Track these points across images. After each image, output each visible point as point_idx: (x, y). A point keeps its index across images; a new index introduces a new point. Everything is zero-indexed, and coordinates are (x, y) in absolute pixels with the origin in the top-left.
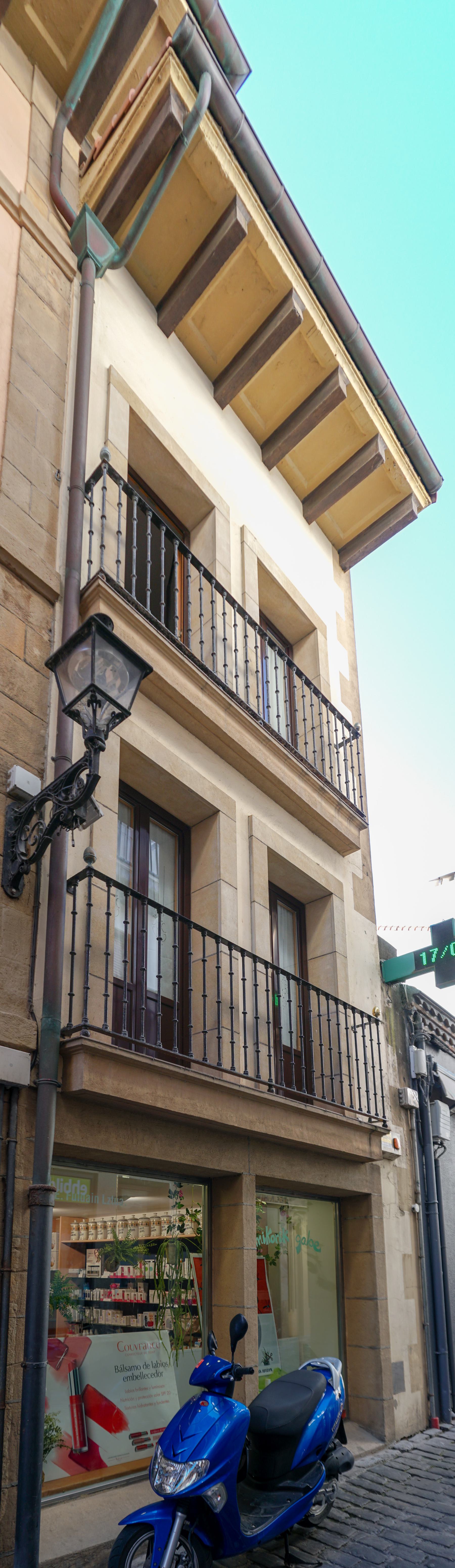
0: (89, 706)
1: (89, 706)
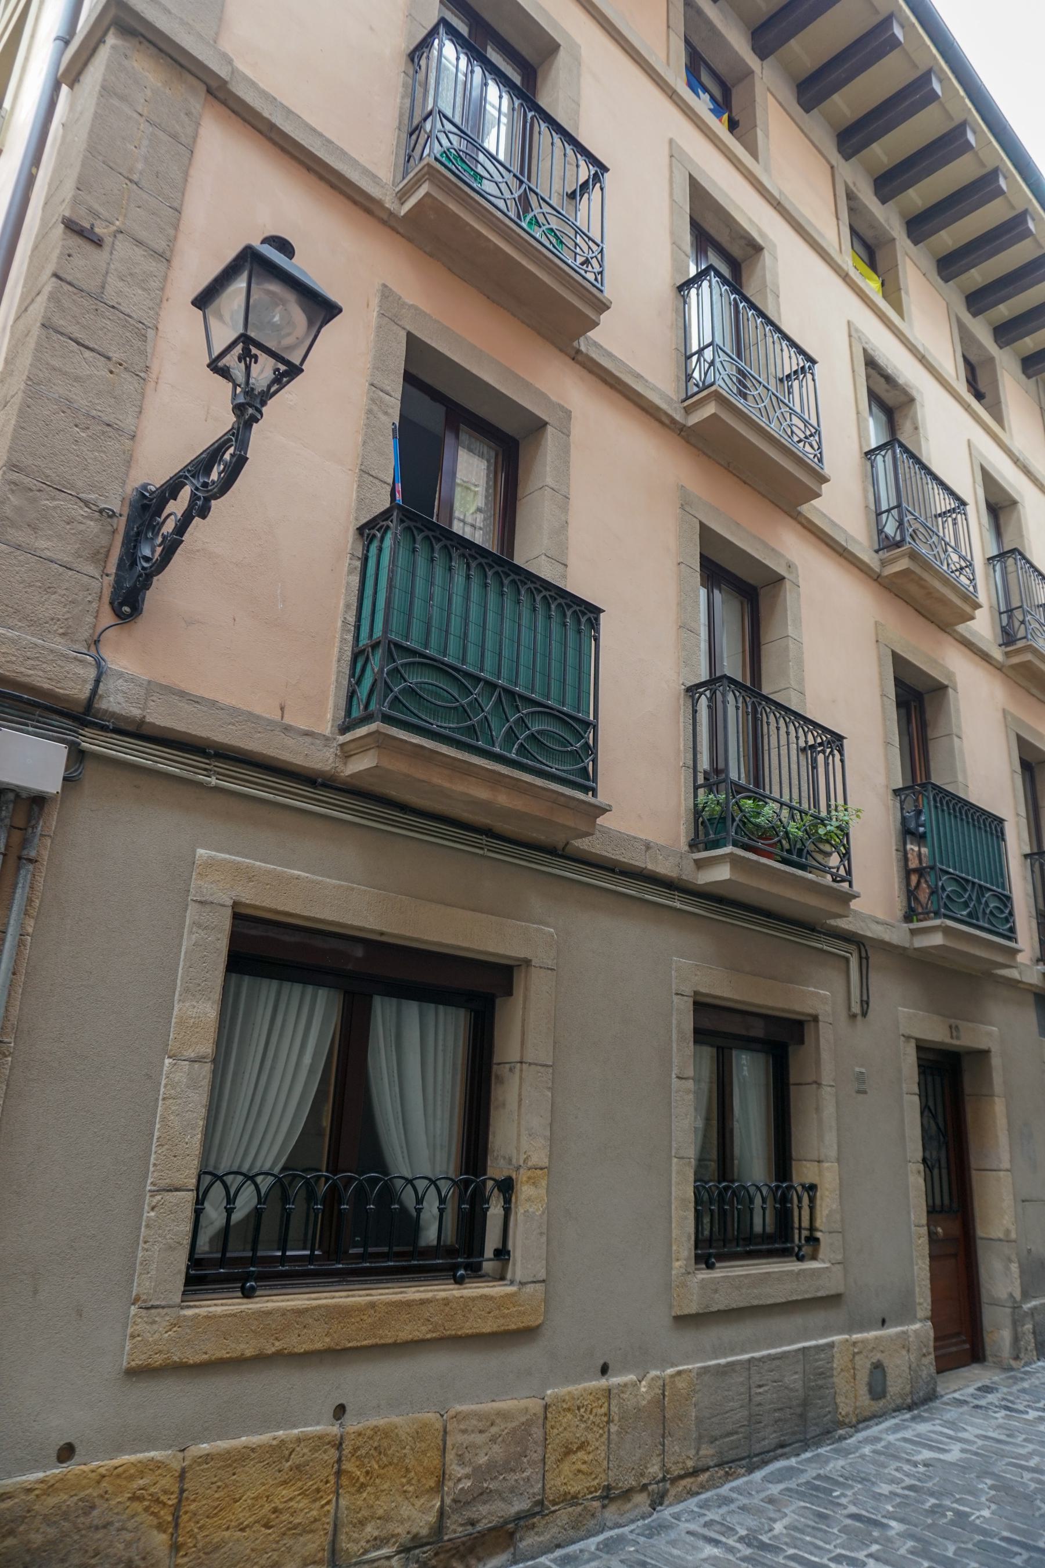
0: (240, 361)
1: (240, 361)
